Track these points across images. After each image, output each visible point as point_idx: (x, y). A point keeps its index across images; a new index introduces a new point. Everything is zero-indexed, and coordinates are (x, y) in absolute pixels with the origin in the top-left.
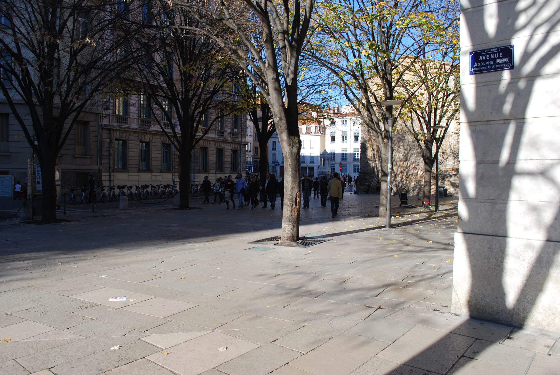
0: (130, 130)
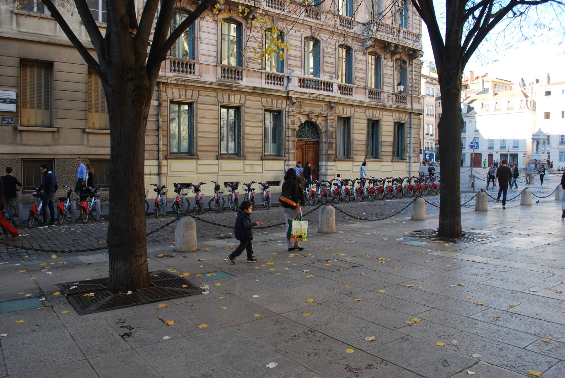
0: (200, 85)
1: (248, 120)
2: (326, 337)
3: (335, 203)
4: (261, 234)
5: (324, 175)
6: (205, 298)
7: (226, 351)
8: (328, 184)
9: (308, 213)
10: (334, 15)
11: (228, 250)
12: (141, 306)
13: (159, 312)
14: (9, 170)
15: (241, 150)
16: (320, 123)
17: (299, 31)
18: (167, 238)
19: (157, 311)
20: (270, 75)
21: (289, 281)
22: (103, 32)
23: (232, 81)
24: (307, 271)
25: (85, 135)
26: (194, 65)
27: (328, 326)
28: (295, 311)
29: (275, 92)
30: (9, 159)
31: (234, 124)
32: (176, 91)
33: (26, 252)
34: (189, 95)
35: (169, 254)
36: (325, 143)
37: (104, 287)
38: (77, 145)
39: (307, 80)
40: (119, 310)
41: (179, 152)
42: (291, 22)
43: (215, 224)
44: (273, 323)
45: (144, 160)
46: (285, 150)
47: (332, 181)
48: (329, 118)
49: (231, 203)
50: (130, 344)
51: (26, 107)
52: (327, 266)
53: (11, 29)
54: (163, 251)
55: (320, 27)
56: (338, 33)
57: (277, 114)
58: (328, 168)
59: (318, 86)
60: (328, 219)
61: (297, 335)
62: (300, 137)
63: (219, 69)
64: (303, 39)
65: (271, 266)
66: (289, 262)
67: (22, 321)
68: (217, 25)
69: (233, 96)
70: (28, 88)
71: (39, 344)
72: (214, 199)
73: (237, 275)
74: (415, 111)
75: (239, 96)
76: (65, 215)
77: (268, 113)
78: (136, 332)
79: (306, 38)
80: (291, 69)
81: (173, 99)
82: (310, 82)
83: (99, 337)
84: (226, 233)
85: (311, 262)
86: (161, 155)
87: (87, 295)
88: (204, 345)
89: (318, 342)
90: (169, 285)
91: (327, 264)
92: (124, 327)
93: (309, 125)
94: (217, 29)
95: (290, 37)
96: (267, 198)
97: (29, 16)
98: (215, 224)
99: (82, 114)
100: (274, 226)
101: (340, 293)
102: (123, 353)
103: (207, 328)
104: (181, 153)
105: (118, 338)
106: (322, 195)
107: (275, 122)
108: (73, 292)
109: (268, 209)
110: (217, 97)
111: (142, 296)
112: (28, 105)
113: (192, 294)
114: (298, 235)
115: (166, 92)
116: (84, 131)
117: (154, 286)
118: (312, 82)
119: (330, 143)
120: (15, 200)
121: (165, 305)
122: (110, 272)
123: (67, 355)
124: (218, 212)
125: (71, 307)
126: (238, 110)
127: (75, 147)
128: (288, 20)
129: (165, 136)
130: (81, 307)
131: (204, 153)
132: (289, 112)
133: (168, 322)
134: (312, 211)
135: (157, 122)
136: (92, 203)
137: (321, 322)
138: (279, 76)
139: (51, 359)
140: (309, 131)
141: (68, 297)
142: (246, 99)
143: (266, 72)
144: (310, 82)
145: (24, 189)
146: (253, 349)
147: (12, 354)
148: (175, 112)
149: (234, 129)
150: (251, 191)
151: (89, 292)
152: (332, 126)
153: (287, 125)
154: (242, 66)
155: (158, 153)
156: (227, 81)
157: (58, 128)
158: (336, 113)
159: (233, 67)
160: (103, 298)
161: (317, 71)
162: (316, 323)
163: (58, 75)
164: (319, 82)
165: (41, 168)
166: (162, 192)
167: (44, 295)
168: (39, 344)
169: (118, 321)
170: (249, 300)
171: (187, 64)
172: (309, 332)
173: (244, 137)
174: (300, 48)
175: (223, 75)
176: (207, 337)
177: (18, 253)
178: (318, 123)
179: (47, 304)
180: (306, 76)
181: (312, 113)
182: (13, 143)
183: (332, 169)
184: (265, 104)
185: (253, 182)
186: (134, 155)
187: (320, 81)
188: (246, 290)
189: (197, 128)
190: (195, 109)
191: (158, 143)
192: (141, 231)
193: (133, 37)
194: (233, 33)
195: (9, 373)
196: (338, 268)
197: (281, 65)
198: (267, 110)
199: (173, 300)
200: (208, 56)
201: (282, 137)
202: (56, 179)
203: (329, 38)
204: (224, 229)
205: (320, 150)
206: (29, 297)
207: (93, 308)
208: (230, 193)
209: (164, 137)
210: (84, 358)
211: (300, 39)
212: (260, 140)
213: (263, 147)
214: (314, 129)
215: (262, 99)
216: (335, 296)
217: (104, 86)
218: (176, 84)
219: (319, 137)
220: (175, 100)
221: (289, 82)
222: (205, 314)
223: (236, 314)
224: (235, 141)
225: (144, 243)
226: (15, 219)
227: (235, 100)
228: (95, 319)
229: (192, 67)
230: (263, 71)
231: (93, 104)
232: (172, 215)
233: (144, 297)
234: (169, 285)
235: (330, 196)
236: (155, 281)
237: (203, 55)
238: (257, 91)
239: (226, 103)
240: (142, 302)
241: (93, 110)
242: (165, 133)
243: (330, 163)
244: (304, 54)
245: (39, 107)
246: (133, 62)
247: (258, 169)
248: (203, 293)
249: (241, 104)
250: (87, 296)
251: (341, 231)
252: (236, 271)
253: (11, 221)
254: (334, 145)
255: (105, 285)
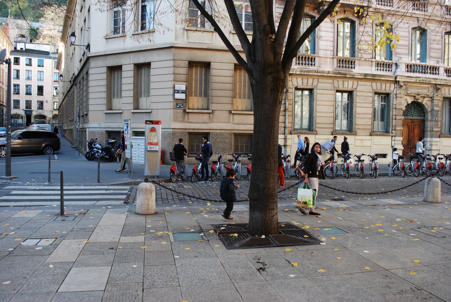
0: (319, 74)
1: (360, 102)
2: (432, 296)
3: (439, 175)
4: (369, 199)
5: (429, 150)
6: (323, 248)
7: (341, 294)
8: (433, 158)
9: (414, 184)
10: (441, 6)
11: (342, 210)
12: (272, 248)
13: (286, 255)
14: (181, 140)
15: (352, 127)
16: (426, 103)
17: (408, 23)
18: (291, 196)
19: (285, 254)
20: (380, 63)
21: (397, 242)
22: (250, 39)
23: (346, 70)
24: (413, 234)
25: (231, 115)
26: (314, 59)
27: (434, 287)
28: (403, 268)
29: (384, 77)
31: (347, 106)
32: (300, 80)
33: (190, 199)
34: (310, 83)
35: (293, 209)
36: (431, 121)
37: (244, 230)
38: (225, 123)
39: (414, 65)
40: (255, 249)
41: (301, 129)
42: (400, 16)
43: (331, 188)
44: (382, 276)
45: (278, 134)
46: (392, 127)
47: (436, 156)
48: (435, 98)
49: (343, 171)
50: (264, 276)
51: (192, 96)
52: (432, 232)
53: (184, 41)
54: (288, 207)
55: (428, 18)
56: (446, 22)
57: (386, 97)
58: (433, 143)
59: (425, 70)
60: (434, 190)
61: (404, 290)
62: (407, 116)
63: (335, 60)
64: (410, 30)
65: (380, 228)
66: (396, 225)
67: (188, 249)
68: (334, 25)
69: (347, 82)
70: (194, 82)
71: (200, 267)
72: (329, 167)
73: (350, 232)
75: (352, 82)
76: (216, 174)
77: (377, 96)
78: (268, 268)
79: (413, 29)
80: (399, 57)
81: (297, 87)
82: (417, 67)
83: (241, 268)
84: (339, 196)
85: (417, 227)
86: (287, 131)
87: (232, 235)
88: (322, 287)
89: (425, 300)
90: (294, 234)
91: (433, 231)
92: (259, 263)
93: (416, 105)
94: (334, 28)
95: (398, 29)
96: (375, 169)
97: (196, 31)
98: (331, 188)
99: (229, 100)
100: (382, 193)
101: (446, 258)
102: (259, 283)
103: (324, 273)
104: (302, 129)
105: (255, 270)
106: (427, 168)
107: (383, 103)
108: (222, 231)
109: (375, 178)
110: (333, 83)
111: (273, 240)
112: (193, 94)
113: (312, 243)
114: (303, 201)
115: (292, 81)
116: (230, 112)
117: (282, 234)
118: (419, 67)
119: (435, 121)
120: (184, 162)
121: (291, 250)
122: (250, 220)
123: (219, 278)
124: (332, 178)
125: (221, 243)
126: (350, 93)
127: (225, 124)
128: (398, 15)
129: (290, 116)
130: (228, 243)
131: (320, 129)
132: (396, 94)
133: (293, 263)
134: (418, 182)
135: (284, 105)
136: (235, 166)
137: (428, 282)
138: (388, 64)
139: (208, 279)
140: (415, 111)
141: (219, 235)
142: (358, 84)
143: (376, 61)
144: (417, 67)
145: (189, 154)
146: (364, 296)
147: (182, 271)
148: (299, 96)
149: (346, 109)
150: (361, 162)
151: (234, 233)
152: (437, 106)
153: (394, 106)
154: (355, 57)
155: (285, 129)
156: (342, 70)
157: (213, 110)
158: (442, 94)
159: (347, 58)
160: (244, 239)
161: (423, 57)
162: (423, 282)
163: (213, 72)
164: (425, 66)
165: (203, 139)
166: (287, 160)
167: (203, 231)
168: (200, 267)
169: (255, 258)
170: (360, 254)
171: (308, 58)
172: (416, 290)
173: (355, 116)
174: (407, 38)
175: (338, 65)
176: (325, 280)
177: (185, 199)
178: (424, 103)
179: (205, 238)
180: (413, 62)
181: (418, 95)
182: (183, 121)
183: (437, 145)
184: (374, 88)
185: (363, 155)
186: (271, 131)
187: (426, 66)
188: (358, 245)
189: (316, 109)
190: (315, 94)
192: (274, 190)
193: (272, 40)
194: (348, 30)
195: (181, 285)
196: (444, 235)
197: (390, 55)
198: (376, 93)
199: (296, 247)
200: (326, 50)
201: (390, 116)
202: (212, 148)
203: (437, 27)
204: (337, 192)
205: (426, 127)
206: (193, 232)
207: (237, 245)
208: (343, 163)
209: (290, 117)
210: (231, 282)
211: (408, 30)
212: (370, 118)
213: (373, 125)
214: (420, 109)
215: (372, 84)
216: (441, 260)
217: (250, 79)
218: (300, 74)
219: (424, 116)
220: (299, 87)
221: (396, 68)
222: (323, 261)
223: (349, 265)
224: (347, 120)
225: (276, 199)
226: (183, 175)
227: (348, 85)
228: (238, 254)
229: (313, 60)
230: (373, 60)
231: (238, 92)
232: (294, 178)
233: (274, 242)
234: (294, 234)
235: (434, 168)
236: (283, 229)
237: (322, 50)
238: (368, 77)
239: (341, 88)
240: (273, 245)
241: (237, 96)
242: (290, 113)
243: (434, 139)
244: (412, 43)
245: (201, 96)
246: (272, 60)
247: (368, 143)
248: (321, 243)
249: (354, 88)
250: (232, 236)
251: (446, 201)
252: (349, 229)
253: (180, 176)
254: (439, 123)
255: (245, 229)
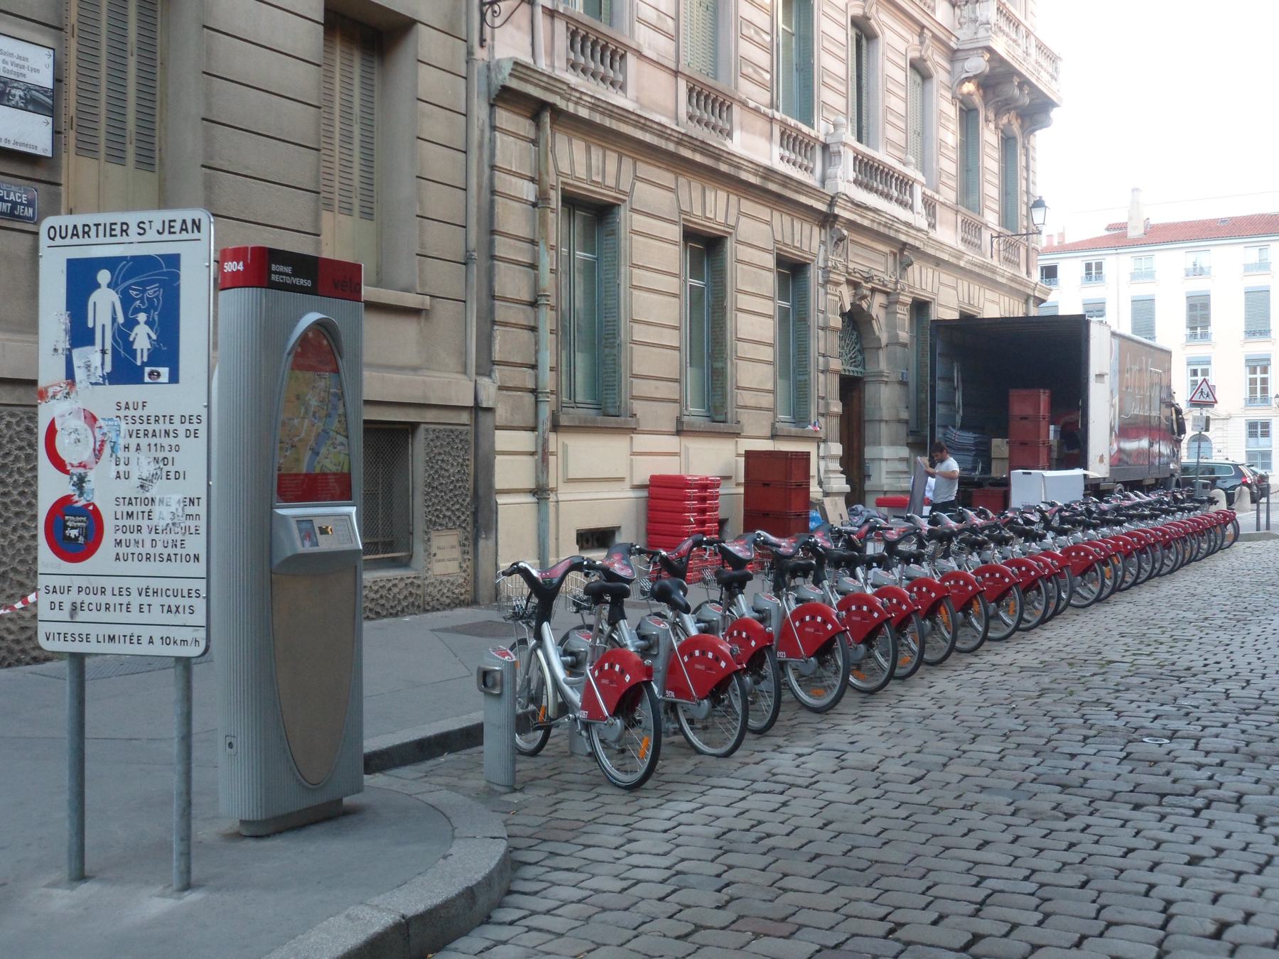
0: (648, 138)
30: (17, 410)
74: (1039, 291)
155: (537, 402)
191: (537, 361)
